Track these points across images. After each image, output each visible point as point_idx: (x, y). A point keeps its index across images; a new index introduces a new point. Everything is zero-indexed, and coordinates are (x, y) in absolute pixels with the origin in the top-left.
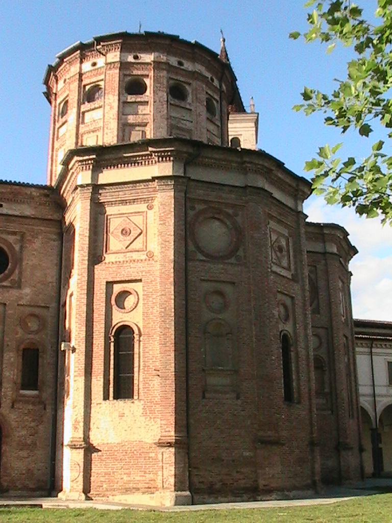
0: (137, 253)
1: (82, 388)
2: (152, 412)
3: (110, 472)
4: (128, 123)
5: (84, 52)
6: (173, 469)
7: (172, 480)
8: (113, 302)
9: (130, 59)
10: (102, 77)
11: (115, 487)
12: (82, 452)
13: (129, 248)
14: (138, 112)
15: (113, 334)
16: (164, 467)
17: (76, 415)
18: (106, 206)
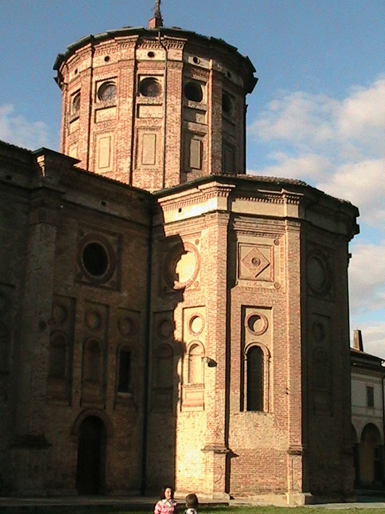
0: (265, 282)
1: (223, 399)
2: (282, 424)
3: (246, 474)
4: (189, 130)
5: (142, 38)
6: (300, 473)
7: (300, 483)
8: (246, 324)
9: (191, 60)
10: (163, 72)
11: (251, 488)
12: (224, 456)
13: (258, 277)
14: (196, 120)
15: (246, 353)
16: (294, 472)
17: (218, 424)
18: (238, 234)
